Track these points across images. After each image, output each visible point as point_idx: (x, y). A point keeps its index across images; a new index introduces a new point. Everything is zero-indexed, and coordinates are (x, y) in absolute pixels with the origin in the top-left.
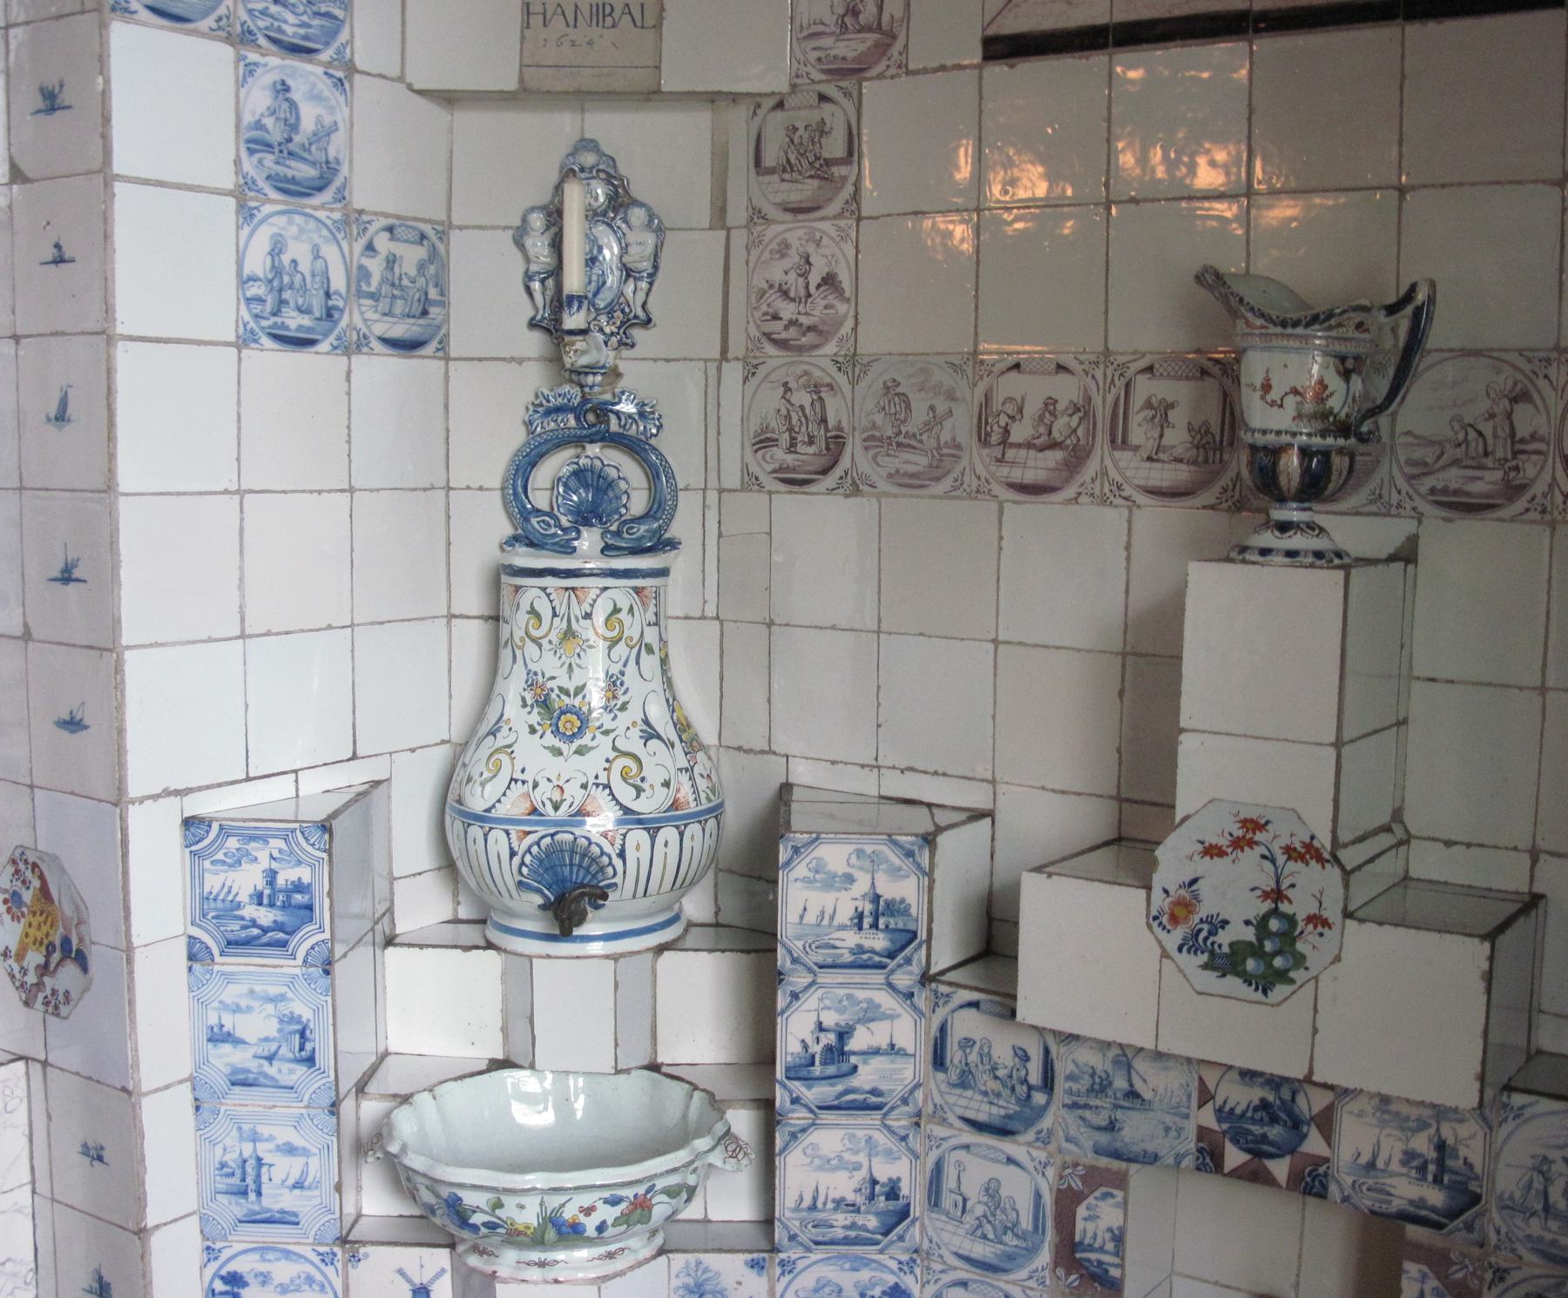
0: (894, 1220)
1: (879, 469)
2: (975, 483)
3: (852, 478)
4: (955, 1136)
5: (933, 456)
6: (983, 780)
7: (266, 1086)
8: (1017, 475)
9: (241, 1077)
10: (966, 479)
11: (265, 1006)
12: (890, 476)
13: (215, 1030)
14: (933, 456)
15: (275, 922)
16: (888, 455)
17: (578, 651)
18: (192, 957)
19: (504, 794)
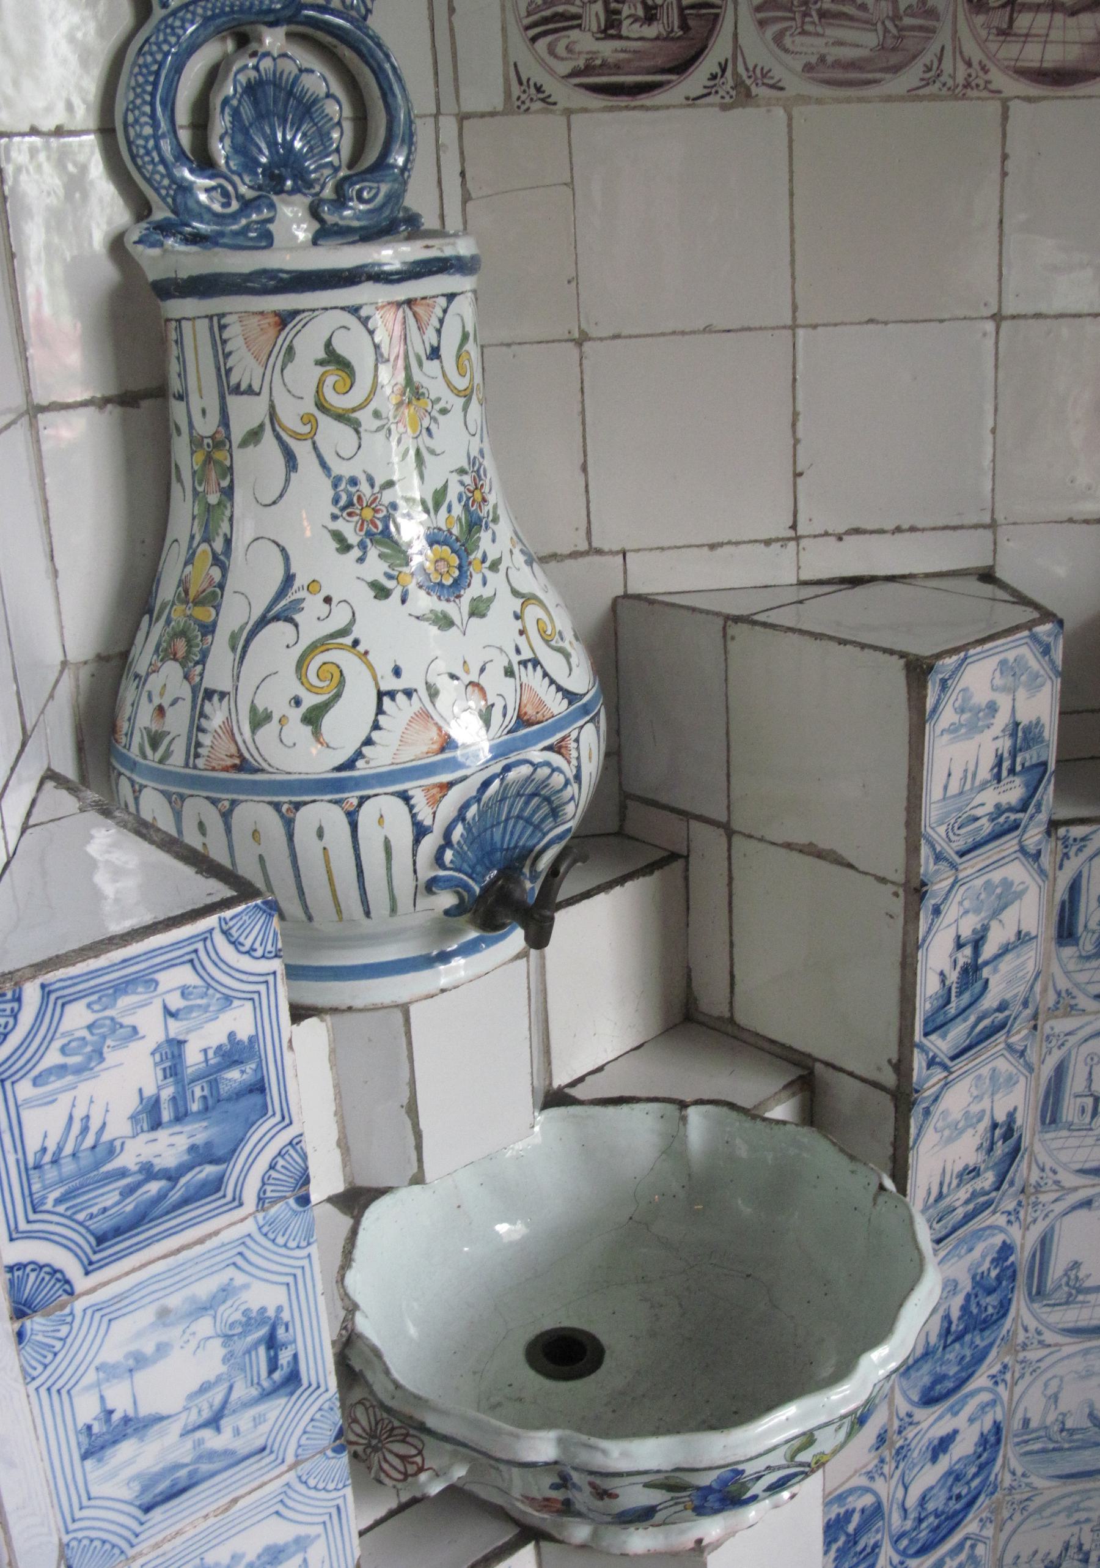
0: (1008, 1162)
1: (787, 58)
2: (962, 72)
3: (735, 73)
4: (1091, 1023)
5: (886, 31)
6: (976, 527)
7: (212, 1475)
8: (1033, 55)
9: (163, 1486)
10: (947, 65)
11: (194, 1327)
12: (808, 68)
13: (96, 1429)
14: (886, 31)
15: (193, 1148)
16: (803, 33)
17: (426, 422)
18: (21, 1311)
19: (376, 726)
